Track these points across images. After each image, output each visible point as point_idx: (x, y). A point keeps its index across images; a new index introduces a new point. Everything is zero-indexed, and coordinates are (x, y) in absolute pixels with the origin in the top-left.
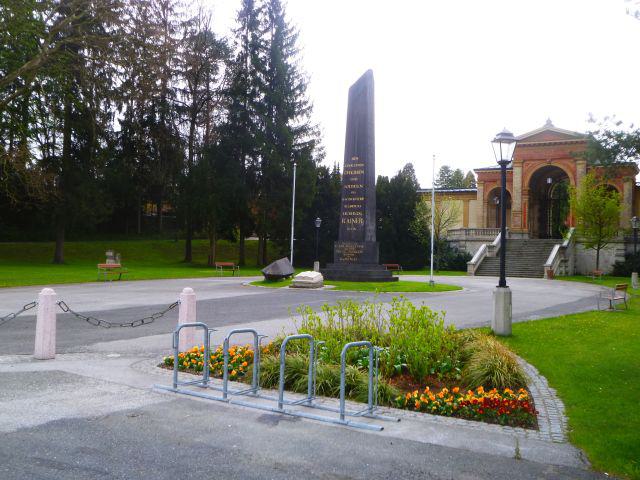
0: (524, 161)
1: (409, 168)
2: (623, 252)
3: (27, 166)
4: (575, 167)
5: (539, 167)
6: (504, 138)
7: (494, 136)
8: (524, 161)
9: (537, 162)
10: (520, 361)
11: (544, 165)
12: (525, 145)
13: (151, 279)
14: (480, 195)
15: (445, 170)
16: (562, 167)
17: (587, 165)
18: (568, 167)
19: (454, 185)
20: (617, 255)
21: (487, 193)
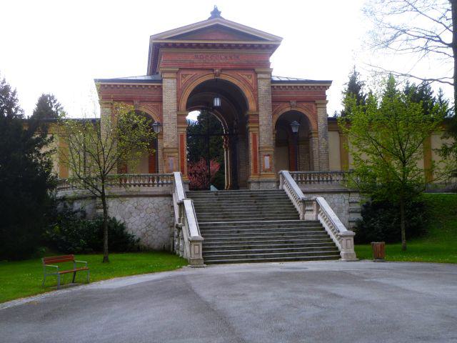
1: (330, 82)
4: (257, 83)
9: (199, 73)
11: (211, 77)
20: (350, 212)
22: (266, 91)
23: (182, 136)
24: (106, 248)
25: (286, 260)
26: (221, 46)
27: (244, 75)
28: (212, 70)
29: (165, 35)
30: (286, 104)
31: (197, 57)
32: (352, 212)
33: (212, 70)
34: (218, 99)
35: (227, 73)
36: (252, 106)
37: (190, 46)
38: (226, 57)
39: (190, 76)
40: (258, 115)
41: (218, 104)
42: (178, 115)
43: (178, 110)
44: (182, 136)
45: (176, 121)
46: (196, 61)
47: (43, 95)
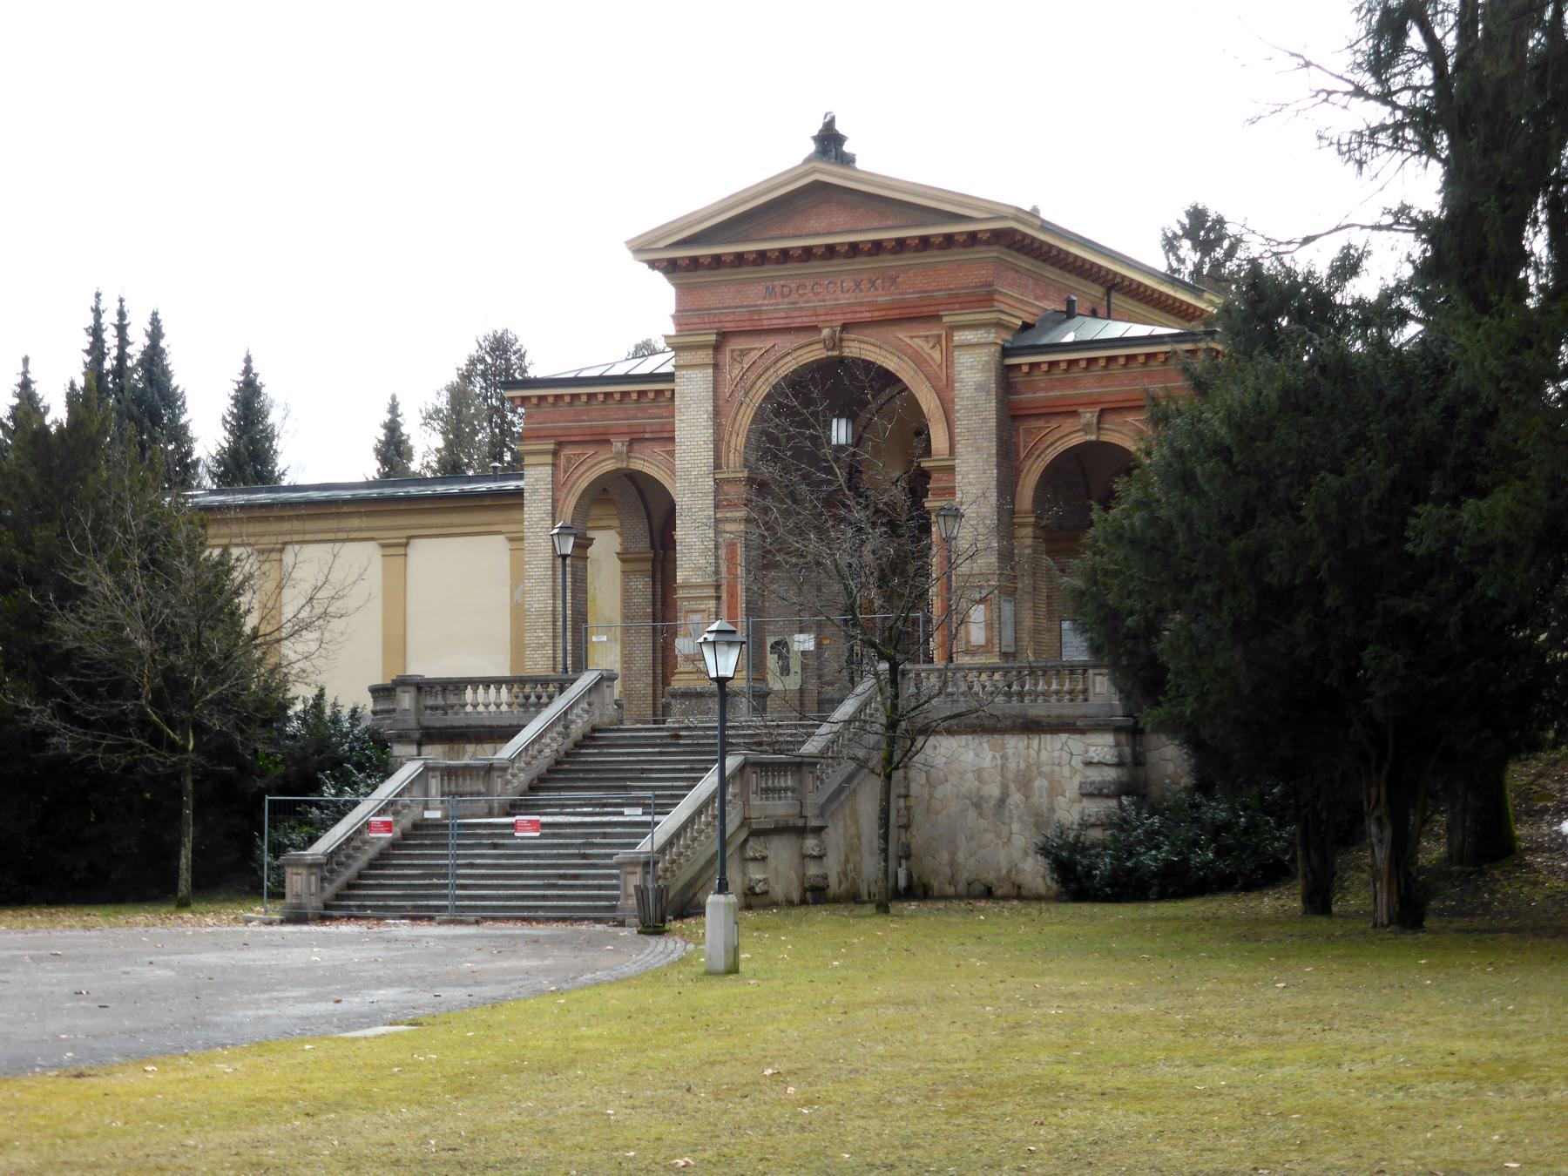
0: (724, 336)
1: (642, 248)
2: (1111, 774)
3: (1531, 303)
4: (949, 361)
5: (788, 366)
6: (1203, 229)
7: (840, 127)
8: (724, 336)
9: (784, 343)
10: (190, 959)
11: (816, 353)
12: (698, 257)
13: (528, 917)
14: (536, 509)
15: (500, 346)
16: (891, 364)
17: (1006, 352)
18: (919, 360)
19: (509, 439)
21: (738, 441)
22: (979, 388)
23: (731, 546)
24: (185, 877)
25: (538, 920)
26: (831, 251)
27: (916, 339)
28: (815, 329)
29: (659, 239)
30: (1069, 424)
31: (770, 292)
32: (1089, 795)
33: (815, 329)
34: (843, 422)
35: (873, 334)
36: (939, 440)
37: (740, 260)
38: (858, 285)
39: (755, 355)
40: (952, 469)
41: (843, 441)
42: (717, 482)
43: (717, 466)
44: (731, 546)
45: (710, 501)
46: (767, 304)
47: (130, 395)
